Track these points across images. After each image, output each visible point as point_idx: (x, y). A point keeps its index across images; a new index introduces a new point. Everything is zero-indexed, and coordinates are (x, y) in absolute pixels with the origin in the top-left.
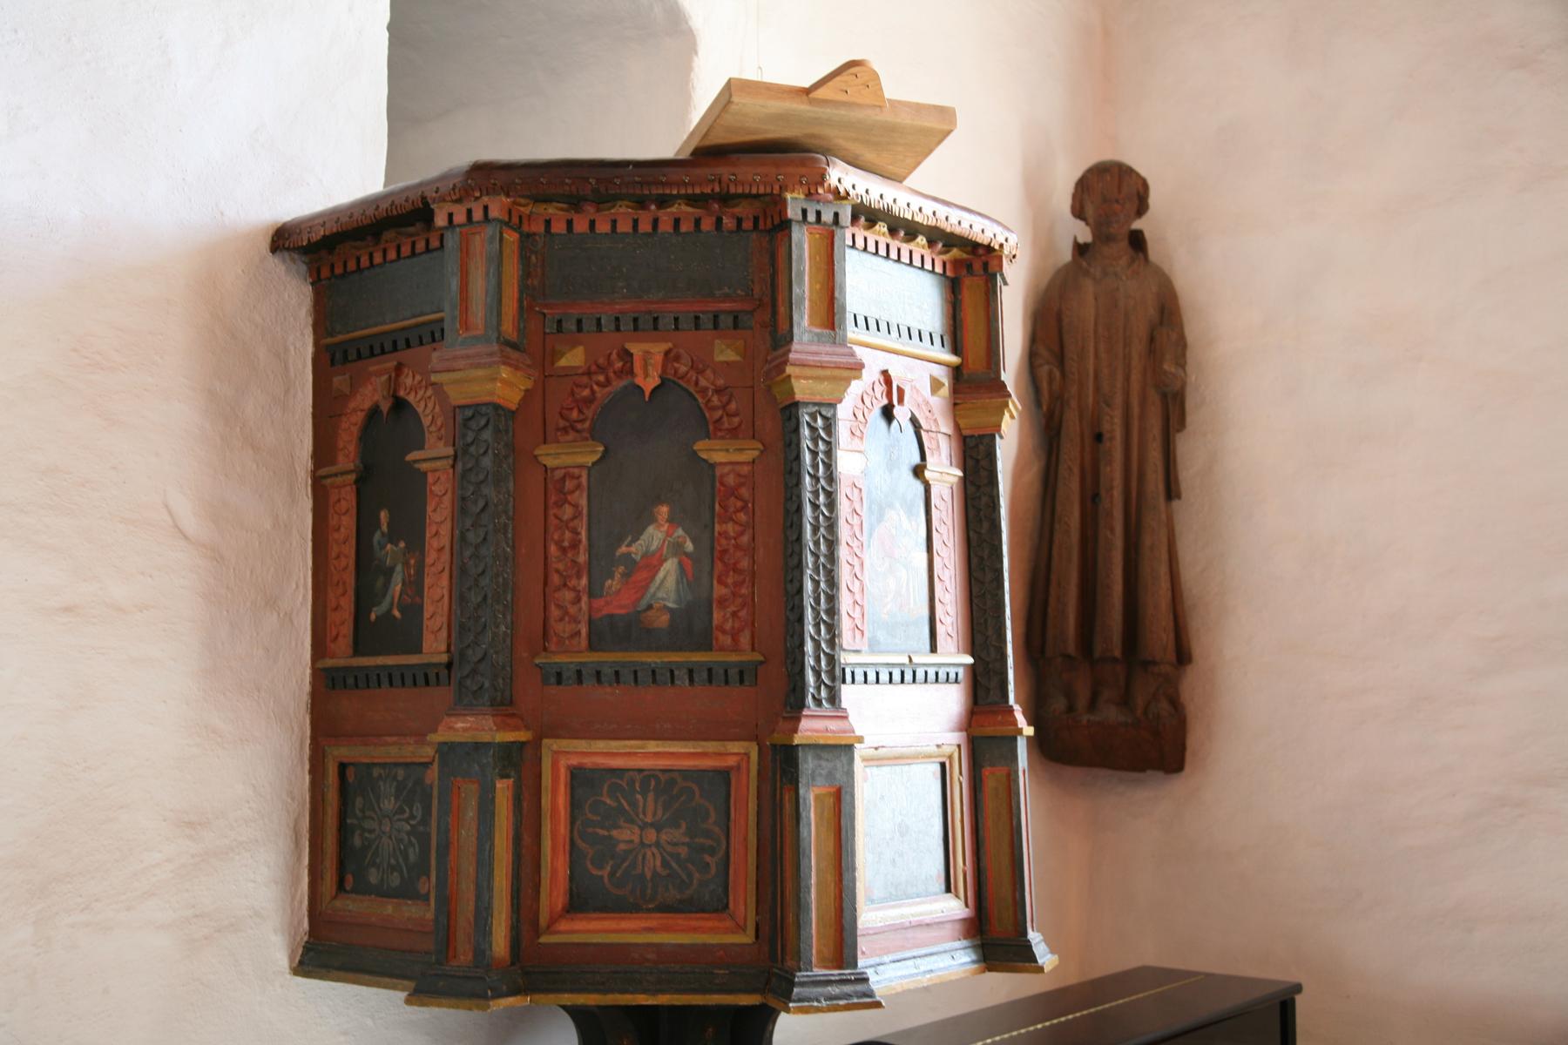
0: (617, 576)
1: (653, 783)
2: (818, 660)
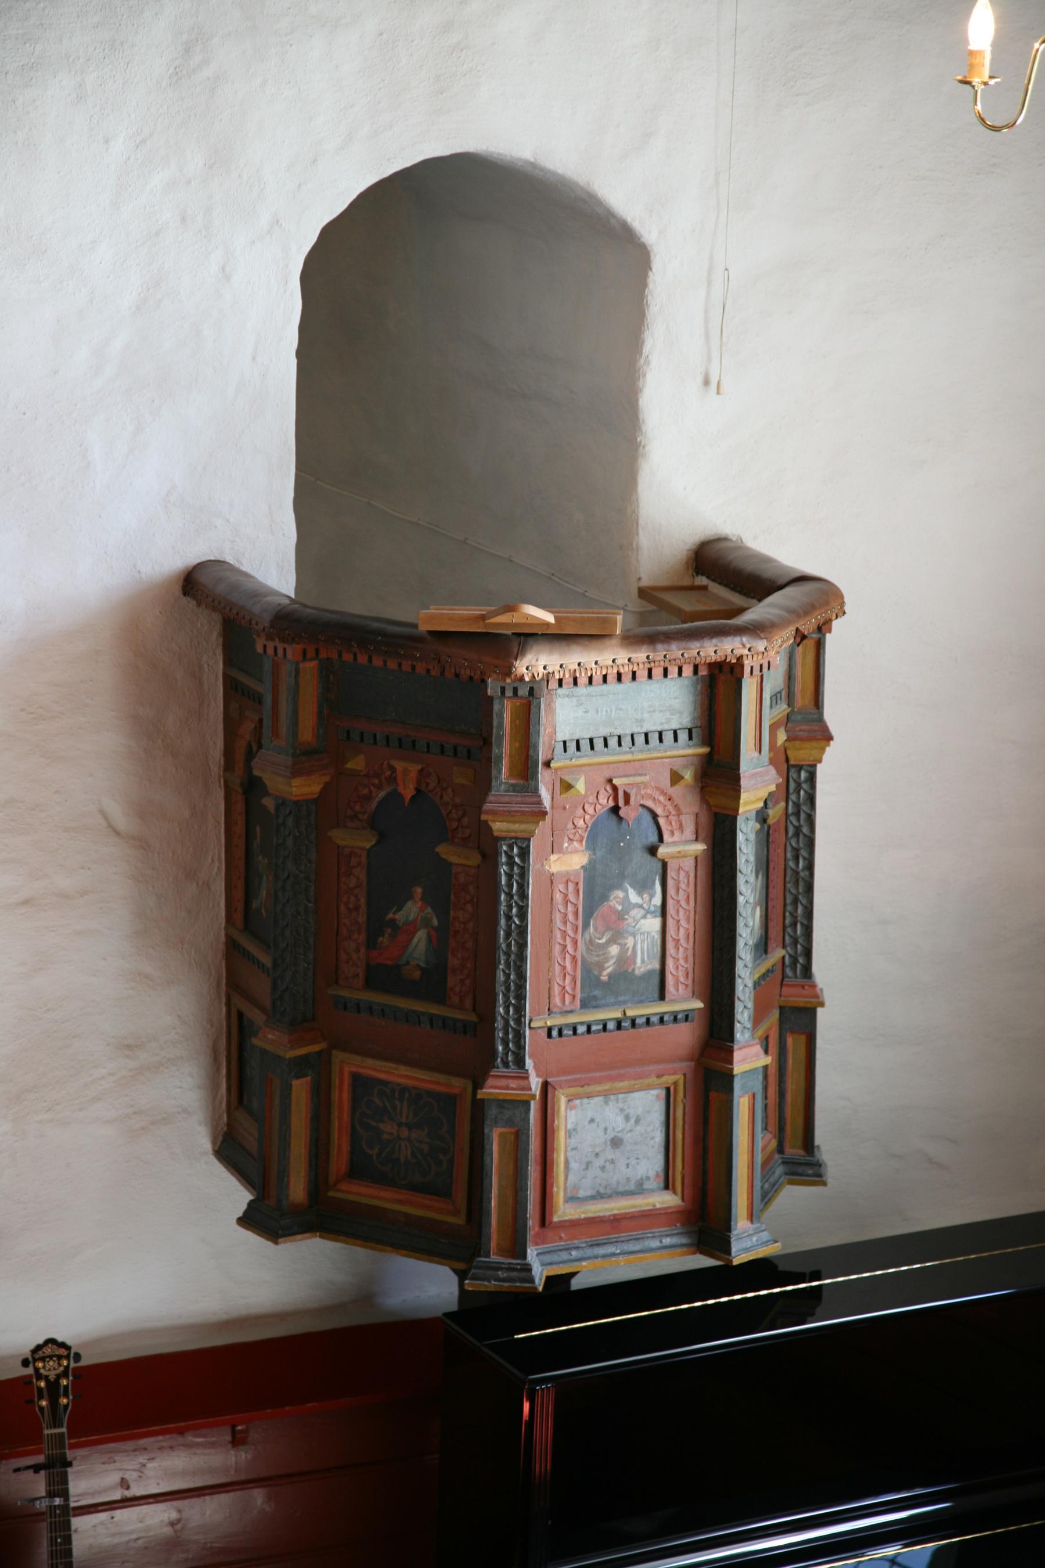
0: (386, 935)
1: (407, 1095)
2: (506, 1033)
